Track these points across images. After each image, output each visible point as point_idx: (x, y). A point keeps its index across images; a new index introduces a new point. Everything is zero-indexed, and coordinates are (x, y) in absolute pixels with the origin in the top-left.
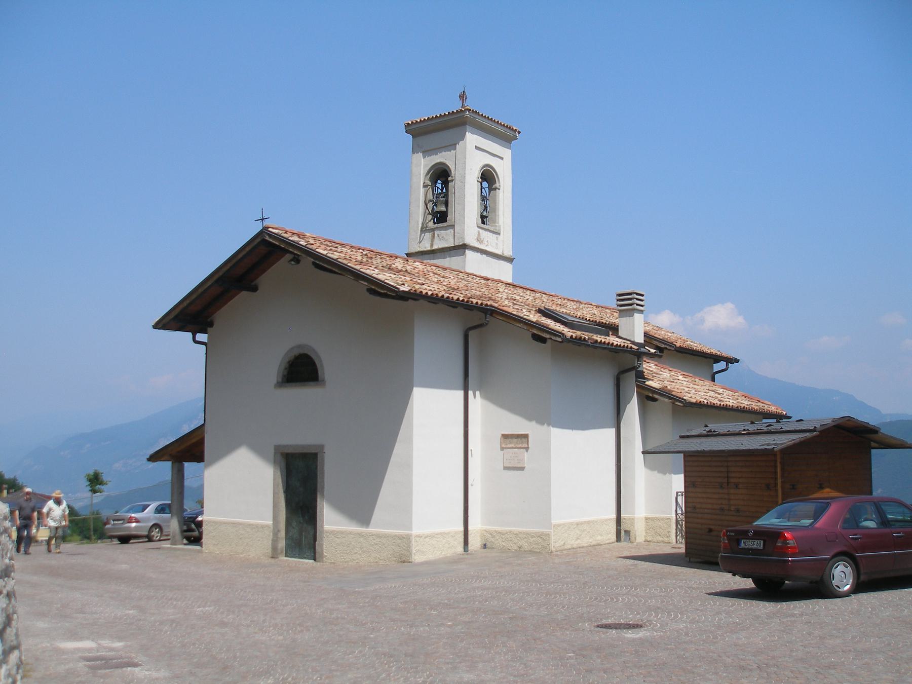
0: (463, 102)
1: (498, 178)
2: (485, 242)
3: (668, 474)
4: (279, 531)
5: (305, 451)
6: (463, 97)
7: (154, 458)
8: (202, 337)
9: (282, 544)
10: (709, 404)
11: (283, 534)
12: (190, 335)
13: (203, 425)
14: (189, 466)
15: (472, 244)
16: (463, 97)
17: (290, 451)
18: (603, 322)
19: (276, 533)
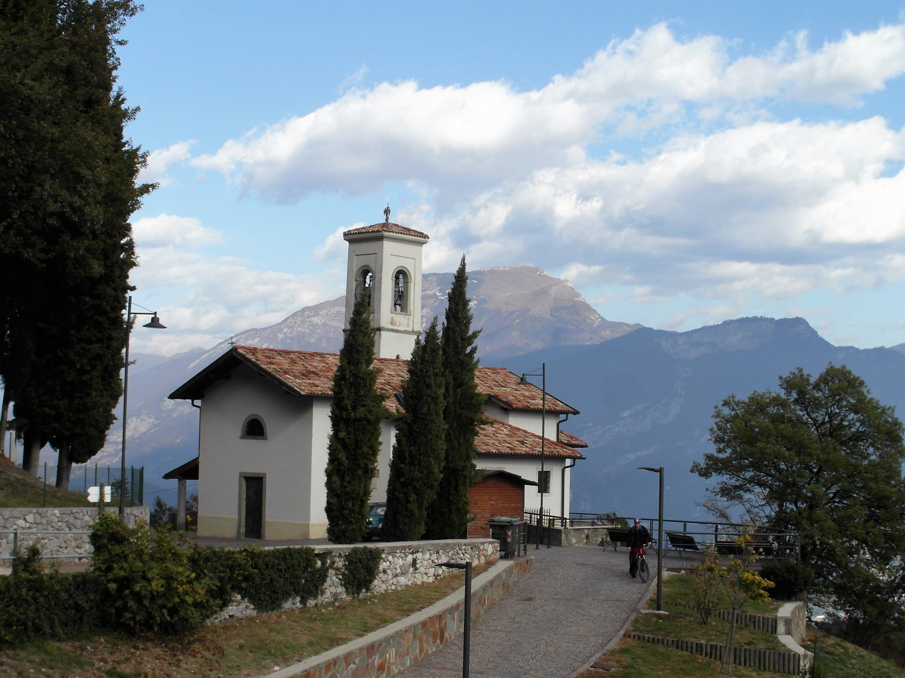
0: (387, 215)
1: (408, 270)
2: (398, 323)
3: (826, 44)
4: (241, 522)
5: (257, 476)
6: (387, 212)
7: (168, 476)
8: (198, 402)
9: (243, 530)
10: (546, 524)
11: (243, 524)
12: (190, 401)
13: (198, 458)
14: (189, 482)
15: (386, 327)
16: (387, 212)
17: (248, 475)
18: (328, 394)
19: (240, 523)
